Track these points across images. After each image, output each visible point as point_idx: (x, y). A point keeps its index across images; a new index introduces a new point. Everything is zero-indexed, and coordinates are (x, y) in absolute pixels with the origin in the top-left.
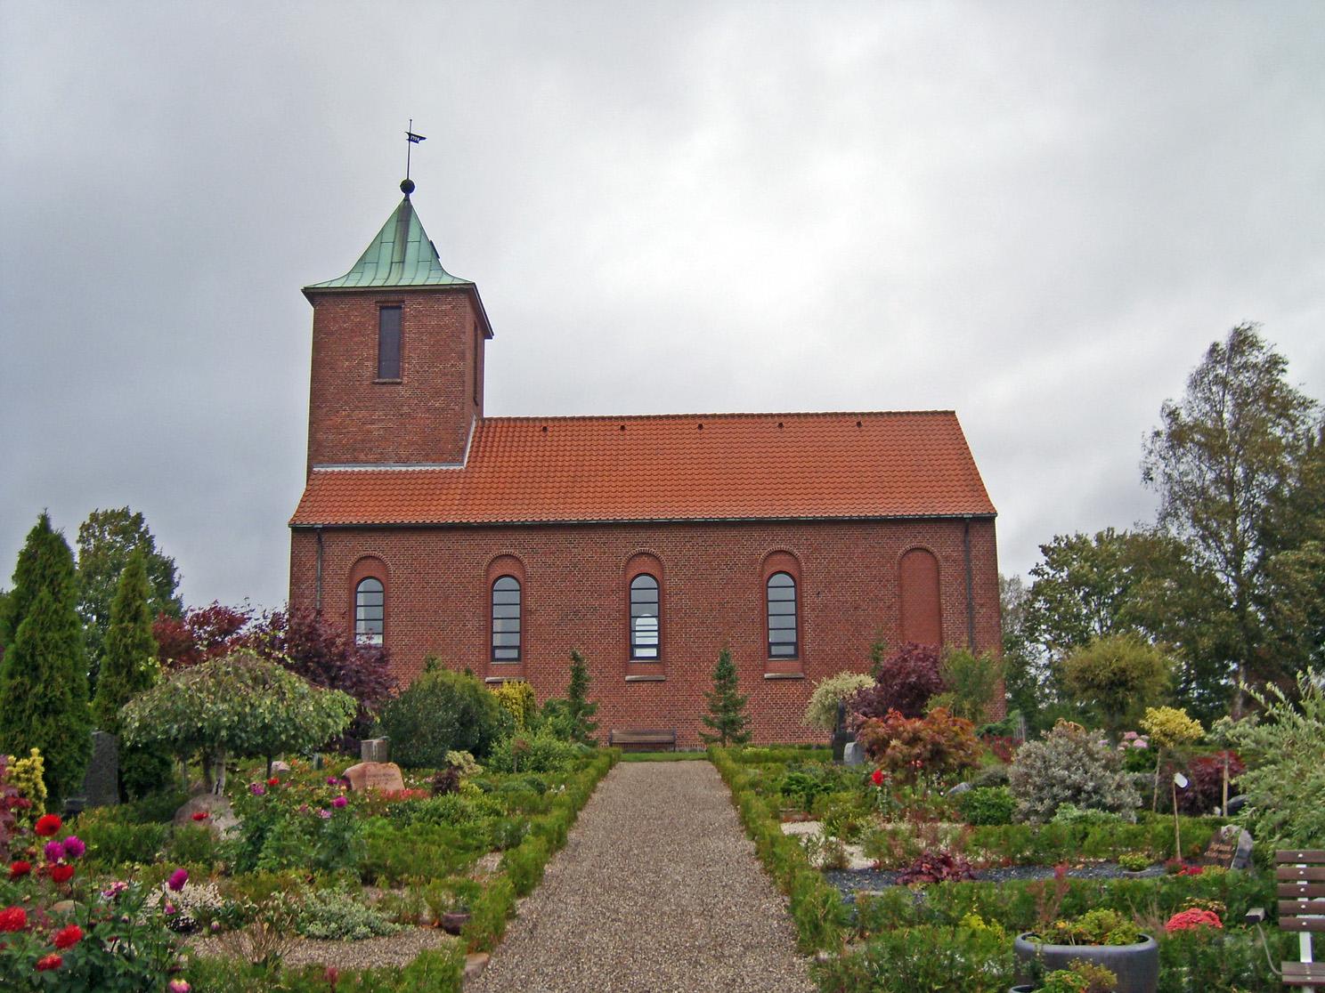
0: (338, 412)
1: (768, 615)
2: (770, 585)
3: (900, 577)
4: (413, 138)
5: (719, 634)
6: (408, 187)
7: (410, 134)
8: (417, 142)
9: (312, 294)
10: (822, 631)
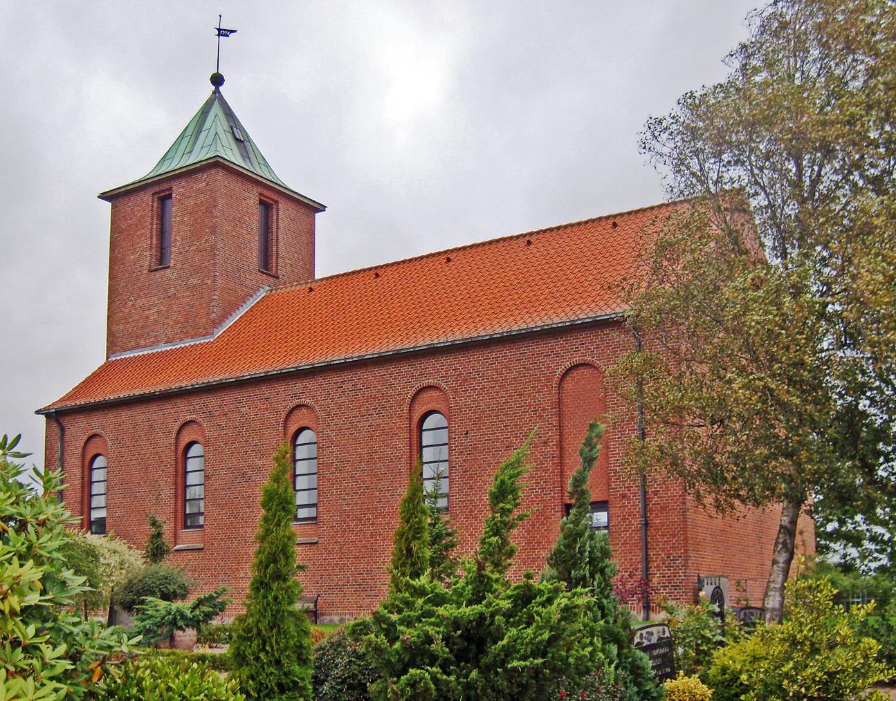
0: (126, 303)
1: (186, 500)
2: (297, 443)
3: (560, 402)
4: (222, 33)
5: (368, 488)
6: (217, 80)
7: (219, 30)
8: (227, 36)
9: (104, 196)
10: (471, 478)
